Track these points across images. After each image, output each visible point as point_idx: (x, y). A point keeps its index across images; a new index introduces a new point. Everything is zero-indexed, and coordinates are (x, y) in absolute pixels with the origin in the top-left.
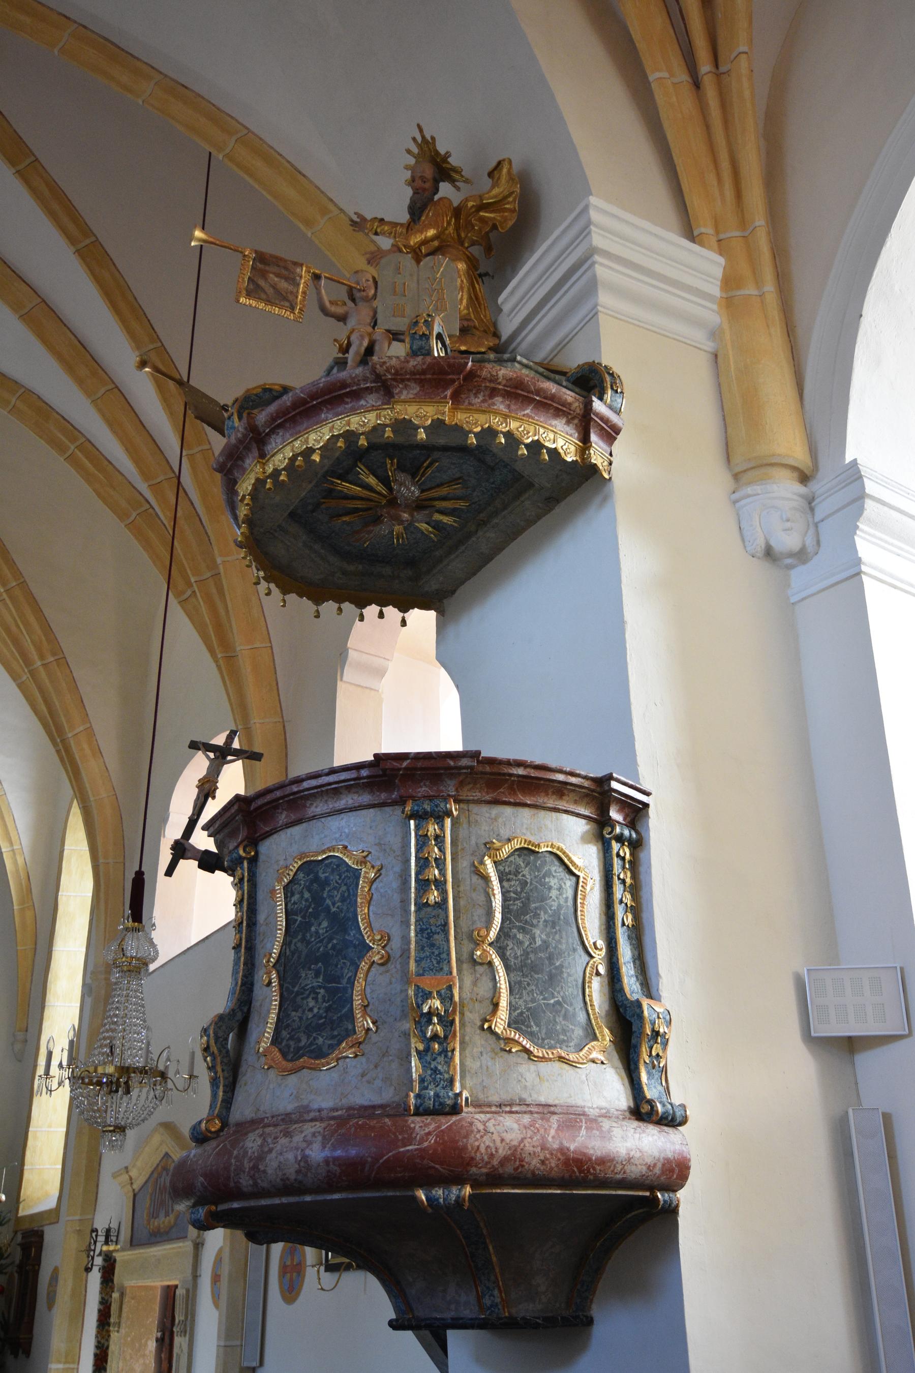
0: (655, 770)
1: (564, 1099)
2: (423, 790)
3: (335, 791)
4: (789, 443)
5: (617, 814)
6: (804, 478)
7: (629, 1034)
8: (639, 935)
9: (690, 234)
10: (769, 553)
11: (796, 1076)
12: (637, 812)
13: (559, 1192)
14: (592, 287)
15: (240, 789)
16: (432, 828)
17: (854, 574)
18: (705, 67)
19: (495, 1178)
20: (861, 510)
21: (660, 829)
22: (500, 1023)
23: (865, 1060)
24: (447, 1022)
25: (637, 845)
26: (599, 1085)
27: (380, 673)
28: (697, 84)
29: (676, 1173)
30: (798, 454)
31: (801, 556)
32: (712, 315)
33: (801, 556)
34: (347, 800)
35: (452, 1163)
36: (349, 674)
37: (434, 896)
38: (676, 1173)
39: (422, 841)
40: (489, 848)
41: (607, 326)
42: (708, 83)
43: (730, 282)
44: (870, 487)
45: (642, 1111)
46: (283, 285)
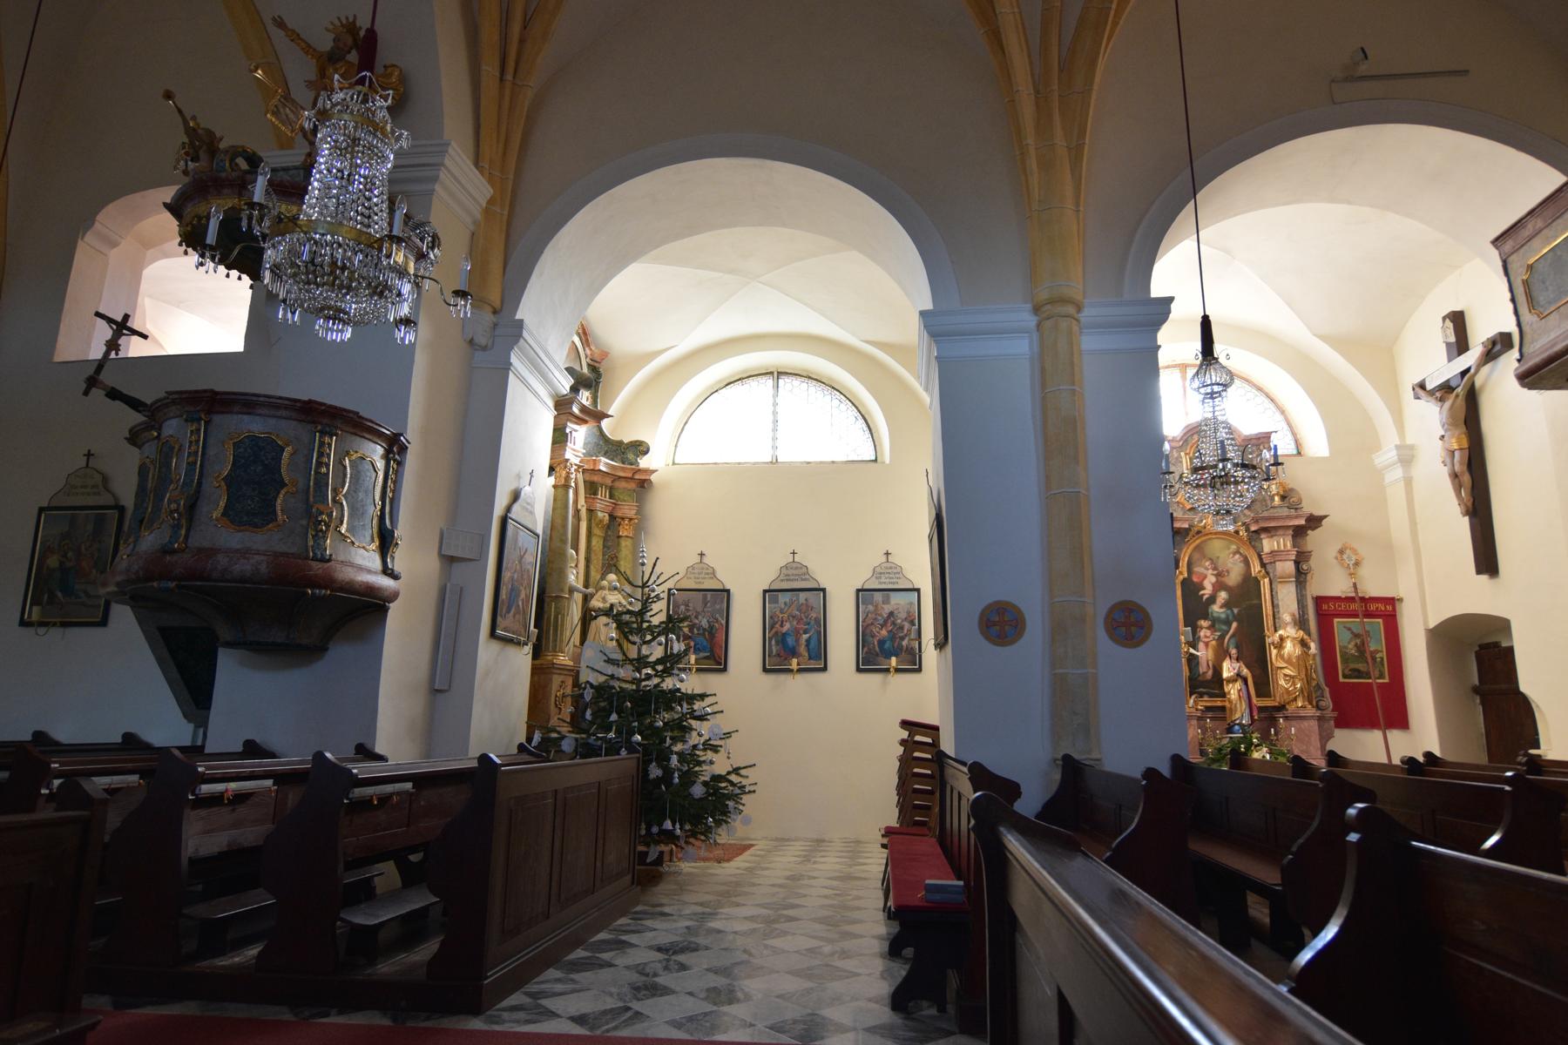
0: (412, 436)
1: (361, 562)
2: (325, 421)
3: (277, 407)
4: (495, 297)
5: (395, 447)
6: (495, 312)
7: (386, 542)
8: (394, 501)
9: (476, 164)
10: (471, 342)
11: (432, 564)
12: (403, 449)
13: (1330, 932)
14: (435, 179)
15: (1267, 911)
16: (327, 439)
17: (507, 366)
18: (509, 77)
19: (341, 589)
20: (517, 342)
21: (411, 460)
22: (343, 530)
23: (455, 565)
24: (328, 526)
25: (399, 464)
26: (374, 561)
27: (114, 244)
28: (501, 80)
29: (394, 596)
30: (497, 304)
31: (484, 348)
32: (478, 215)
33: (484, 348)
34: (284, 413)
35: (329, 582)
36: (89, 237)
37: (324, 470)
38: (394, 596)
39: (322, 444)
40: (348, 453)
41: (436, 206)
42: (508, 85)
43: (491, 201)
44: (525, 334)
45: (387, 571)
46: (291, 116)
